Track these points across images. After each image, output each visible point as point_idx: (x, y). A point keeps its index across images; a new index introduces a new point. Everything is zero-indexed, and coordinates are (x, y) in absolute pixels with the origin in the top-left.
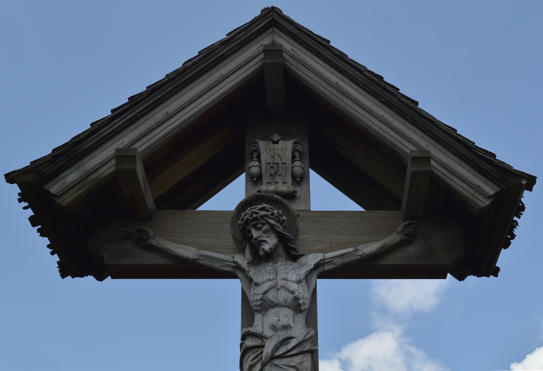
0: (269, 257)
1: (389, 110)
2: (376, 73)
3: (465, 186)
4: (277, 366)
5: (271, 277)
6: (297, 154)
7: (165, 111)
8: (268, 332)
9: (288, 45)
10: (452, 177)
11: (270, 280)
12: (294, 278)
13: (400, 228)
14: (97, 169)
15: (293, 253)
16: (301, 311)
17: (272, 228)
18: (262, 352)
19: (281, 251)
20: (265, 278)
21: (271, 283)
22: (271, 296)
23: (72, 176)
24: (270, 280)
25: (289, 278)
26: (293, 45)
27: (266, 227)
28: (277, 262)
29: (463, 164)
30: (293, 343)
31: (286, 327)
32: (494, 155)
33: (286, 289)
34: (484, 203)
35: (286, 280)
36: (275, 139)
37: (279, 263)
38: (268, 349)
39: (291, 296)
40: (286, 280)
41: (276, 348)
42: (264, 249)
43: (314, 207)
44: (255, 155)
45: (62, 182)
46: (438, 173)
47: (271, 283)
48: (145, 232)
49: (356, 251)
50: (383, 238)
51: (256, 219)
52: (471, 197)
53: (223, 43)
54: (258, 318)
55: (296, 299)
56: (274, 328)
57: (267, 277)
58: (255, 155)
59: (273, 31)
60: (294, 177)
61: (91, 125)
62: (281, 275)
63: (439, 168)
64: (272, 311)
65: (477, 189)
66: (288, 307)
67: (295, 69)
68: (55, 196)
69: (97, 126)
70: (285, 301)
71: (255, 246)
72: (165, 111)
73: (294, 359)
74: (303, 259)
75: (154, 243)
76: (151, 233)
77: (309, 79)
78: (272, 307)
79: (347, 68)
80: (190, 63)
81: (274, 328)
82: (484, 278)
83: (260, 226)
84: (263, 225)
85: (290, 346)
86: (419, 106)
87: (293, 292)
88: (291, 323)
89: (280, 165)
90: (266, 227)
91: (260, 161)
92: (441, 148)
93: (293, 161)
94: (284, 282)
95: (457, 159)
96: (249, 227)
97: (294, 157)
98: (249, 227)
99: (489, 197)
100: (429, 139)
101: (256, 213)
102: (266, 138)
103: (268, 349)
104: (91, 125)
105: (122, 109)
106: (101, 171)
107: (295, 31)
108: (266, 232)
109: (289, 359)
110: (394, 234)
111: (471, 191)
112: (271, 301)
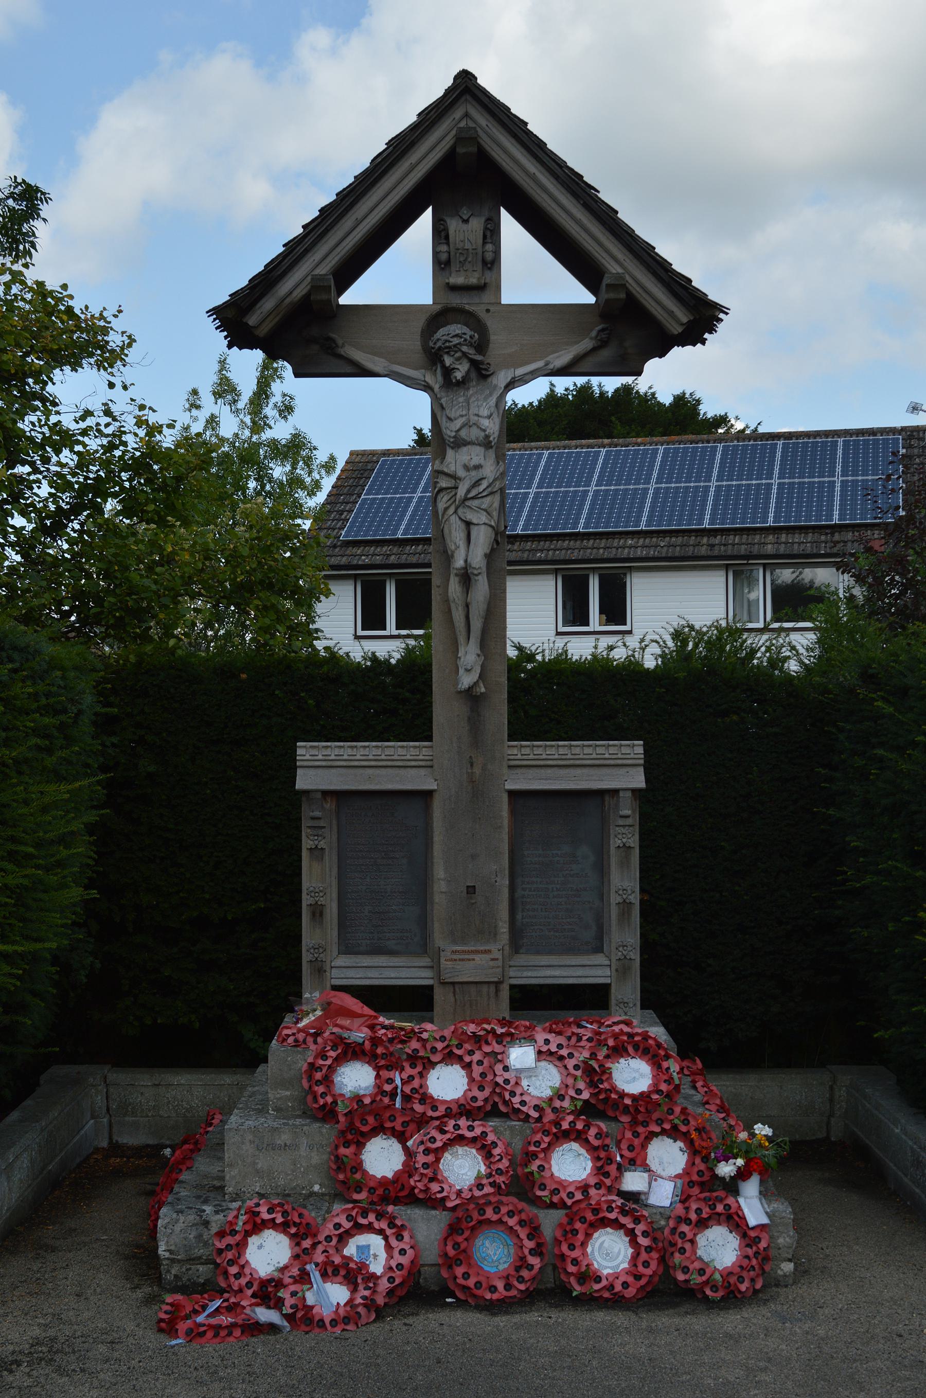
0: (462, 383)
1: (588, 215)
2: (576, 170)
3: (659, 309)
4: (469, 507)
5: (464, 413)
6: (488, 233)
7: (353, 218)
8: (461, 473)
9: (482, 120)
10: (647, 297)
11: (462, 416)
12: (486, 413)
13: (594, 334)
14: (291, 293)
15: (484, 372)
16: (491, 447)
17: (465, 354)
18: (456, 494)
19: (473, 375)
20: (458, 414)
21: (464, 419)
22: (463, 434)
23: (268, 304)
24: (462, 416)
25: (480, 414)
26: (487, 120)
27: (458, 354)
28: (469, 389)
29: (659, 285)
30: (484, 484)
31: (478, 467)
32: (690, 281)
33: (478, 427)
34: (676, 333)
35: (478, 415)
36: (465, 217)
37: (471, 392)
38: (461, 492)
39: (483, 434)
40: (478, 415)
41: (469, 491)
42: (456, 377)
43: (507, 298)
44: (443, 234)
45: (259, 312)
46: (634, 292)
47: (464, 419)
48: (333, 340)
49: (547, 364)
50: (577, 343)
51: (449, 347)
52: (664, 322)
53: (413, 128)
54: (450, 453)
55: (487, 437)
56: (466, 468)
57: (459, 412)
58: (443, 234)
59: (466, 100)
60: (484, 263)
61: (284, 246)
62: (473, 410)
63: (635, 286)
64: (465, 449)
65: (671, 314)
66: (480, 445)
67: (488, 149)
68: (254, 327)
69: (292, 246)
70: (477, 439)
71: (447, 372)
72: (353, 218)
73: (484, 500)
74: (494, 380)
75: (343, 353)
76: (340, 342)
77: (504, 164)
78: (465, 445)
79: (546, 159)
80: (379, 159)
81: (466, 468)
82: (689, 348)
83: (452, 353)
84: (456, 352)
85: (481, 488)
86: (619, 215)
87: (484, 431)
88: (482, 462)
89: (471, 251)
90: (458, 354)
91: (448, 244)
92: (638, 264)
93: (484, 243)
94: (476, 418)
95: (653, 279)
96: (441, 353)
97: (485, 237)
98: (441, 353)
99: (682, 324)
100: (628, 253)
101: (450, 342)
102: (456, 214)
103: (461, 492)
104: (284, 246)
105: (315, 224)
106: (295, 294)
107: (490, 106)
108: (458, 359)
109: (480, 500)
110: (587, 340)
111: (665, 315)
112: (463, 440)
